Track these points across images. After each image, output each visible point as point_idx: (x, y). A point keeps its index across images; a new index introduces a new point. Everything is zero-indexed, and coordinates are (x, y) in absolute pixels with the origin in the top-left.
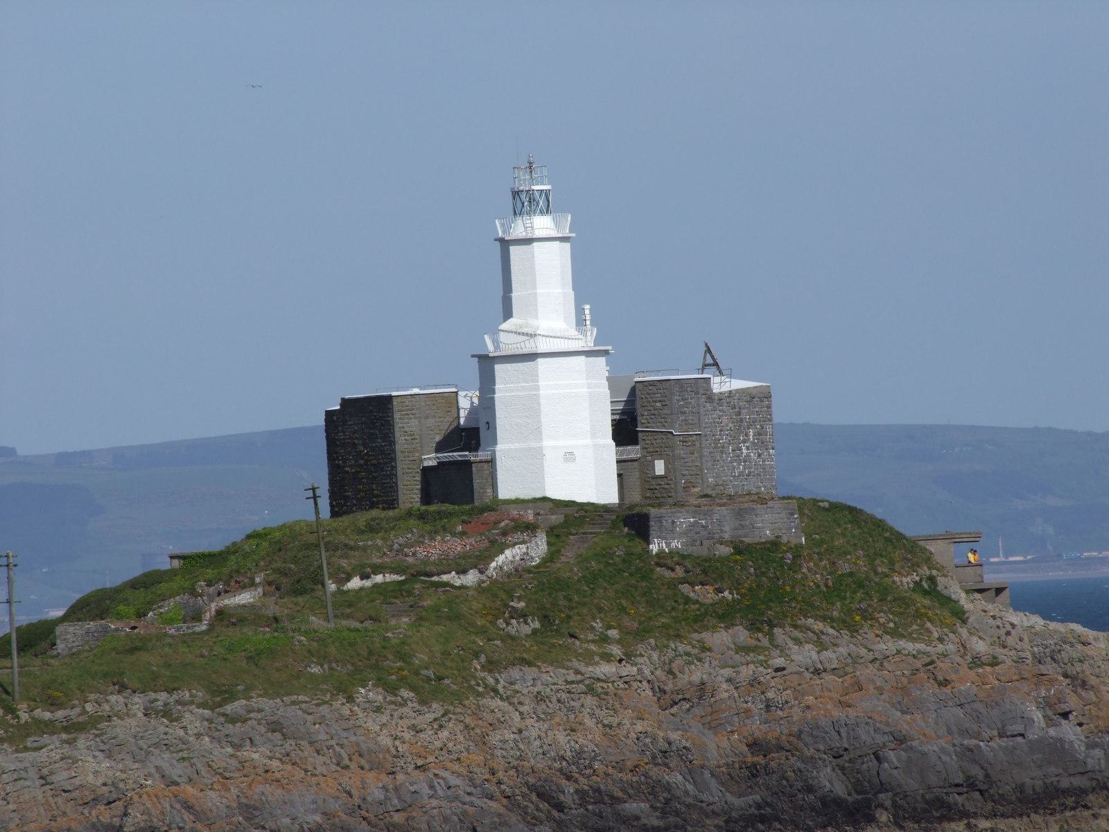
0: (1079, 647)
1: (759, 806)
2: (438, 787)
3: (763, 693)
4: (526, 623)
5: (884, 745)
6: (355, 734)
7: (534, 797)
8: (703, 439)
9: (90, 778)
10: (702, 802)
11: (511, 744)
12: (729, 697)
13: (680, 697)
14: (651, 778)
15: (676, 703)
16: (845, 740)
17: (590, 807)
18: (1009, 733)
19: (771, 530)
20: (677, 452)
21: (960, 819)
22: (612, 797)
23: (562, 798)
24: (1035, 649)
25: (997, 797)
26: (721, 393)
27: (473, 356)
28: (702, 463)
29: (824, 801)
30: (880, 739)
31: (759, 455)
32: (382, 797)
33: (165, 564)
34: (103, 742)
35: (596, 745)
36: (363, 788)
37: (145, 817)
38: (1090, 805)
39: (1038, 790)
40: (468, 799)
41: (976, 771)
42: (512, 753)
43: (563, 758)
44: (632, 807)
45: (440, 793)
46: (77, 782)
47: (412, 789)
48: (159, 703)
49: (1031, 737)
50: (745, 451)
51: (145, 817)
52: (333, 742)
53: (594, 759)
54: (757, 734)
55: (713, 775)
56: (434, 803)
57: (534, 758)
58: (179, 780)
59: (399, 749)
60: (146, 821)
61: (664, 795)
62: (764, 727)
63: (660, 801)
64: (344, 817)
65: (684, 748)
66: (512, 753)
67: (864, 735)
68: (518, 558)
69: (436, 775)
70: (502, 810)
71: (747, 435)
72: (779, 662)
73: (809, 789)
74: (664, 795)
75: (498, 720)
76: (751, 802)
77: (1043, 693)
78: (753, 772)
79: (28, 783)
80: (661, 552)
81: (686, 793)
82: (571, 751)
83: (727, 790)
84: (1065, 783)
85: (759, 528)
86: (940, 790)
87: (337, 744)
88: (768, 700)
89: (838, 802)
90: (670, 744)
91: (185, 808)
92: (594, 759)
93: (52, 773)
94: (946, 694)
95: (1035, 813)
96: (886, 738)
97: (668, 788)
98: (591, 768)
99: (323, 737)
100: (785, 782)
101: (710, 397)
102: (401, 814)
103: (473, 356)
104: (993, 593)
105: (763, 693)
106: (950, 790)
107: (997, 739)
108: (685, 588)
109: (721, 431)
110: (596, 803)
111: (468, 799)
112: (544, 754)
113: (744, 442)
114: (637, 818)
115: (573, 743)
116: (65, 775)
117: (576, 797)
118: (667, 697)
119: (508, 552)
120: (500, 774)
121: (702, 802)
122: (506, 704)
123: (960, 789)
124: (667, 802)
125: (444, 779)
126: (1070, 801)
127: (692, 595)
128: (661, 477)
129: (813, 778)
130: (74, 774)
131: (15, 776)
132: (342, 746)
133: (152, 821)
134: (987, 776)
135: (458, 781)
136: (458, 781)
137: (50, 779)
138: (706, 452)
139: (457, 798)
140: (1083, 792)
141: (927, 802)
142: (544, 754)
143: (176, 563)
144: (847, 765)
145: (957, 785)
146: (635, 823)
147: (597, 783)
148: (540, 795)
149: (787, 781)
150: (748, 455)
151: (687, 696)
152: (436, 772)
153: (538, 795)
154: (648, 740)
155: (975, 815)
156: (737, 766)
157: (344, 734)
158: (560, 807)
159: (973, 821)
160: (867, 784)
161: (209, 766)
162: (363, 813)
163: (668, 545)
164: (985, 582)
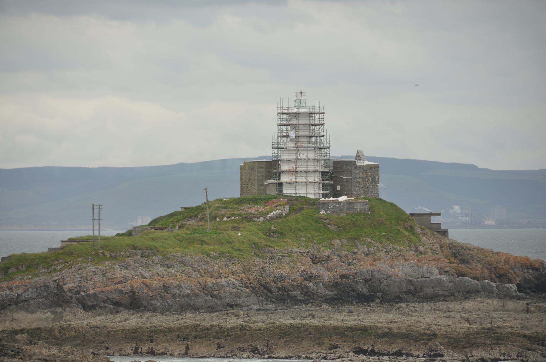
0: (468, 251)
1: (336, 295)
2: (230, 284)
3: (348, 260)
4: (275, 234)
5: (383, 278)
6: (207, 266)
7: (262, 288)
8: (353, 180)
9: (118, 275)
10: (318, 293)
11: (259, 271)
12: (337, 261)
13: (322, 260)
14: (302, 284)
15: (320, 262)
16: (371, 276)
17: (280, 292)
18: (425, 277)
19: (359, 209)
20: (344, 183)
21: (405, 302)
22: (289, 290)
23: (272, 289)
24: (453, 251)
25: (418, 296)
26: (360, 166)
27: (60, 241)
28: (351, 187)
29: (358, 294)
30: (382, 276)
31: (373, 186)
32: (212, 286)
33: (180, 210)
34: (124, 264)
35: (287, 273)
36: (206, 283)
37: (131, 288)
38: (447, 300)
39: (431, 295)
40: (239, 288)
41: (412, 288)
42: (259, 274)
43: (276, 277)
44: (293, 293)
45: (231, 286)
46: (114, 276)
47: (222, 284)
48: (146, 253)
49: (431, 278)
50: (367, 184)
51: (131, 288)
52: (199, 268)
53: (285, 278)
54: (344, 273)
55: (323, 285)
56: (228, 288)
57: (267, 276)
58: (147, 277)
59: (221, 271)
60: (131, 289)
61: (306, 290)
62: (346, 271)
63: (304, 292)
64: (197, 291)
65: (317, 276)
66: (259, 274)
67: (377, 275)
68: (278, 214)
69: (230, 280)
70: (250, 292)
71: (369, 179)
72: (355, 250)
73: (354, 291)
74: (306, 290)
75: (255, 264)
76: (334, 294)
77: (440, 265)
78: (337, 284)
79: (98, 276)
80: (324, 214)
81: (313, 290)
82: (279, 275)
83: (327, 289)
84: (440, 293)
85: (467, 215)
86: (399, 293)
87: (201, 269)
88: (349, 262)
89: (363, 295)
90: (312, 274)
91: (146, 286)
92: (285, 278)
93: (106, 273)
94: (406, 263)
95: (430, 302)
96: (384, 276)
97: (307, 287)
98: (284, 280)
99: (196, 266)
100: (346, 288)
101: (356, 167)
102: (217, 292)
103: (60, 241)
104: (443, 233)
105: (348, 260)
106: (403, 293)
107: (421, 278)
108: (329, 226)
109: (359, 177)
110: (283, 291)
111: (239, 288)
112: (270, 275)
113: (367, 181)
114: (296, 297)
115: (279, 272)
116: (110, 274)
117: (277, 289)
118: (317, 259)
119: (274, 212)
120: (251, 281)
121: (318, 293)
122: (469, 278)
123: (406, 293)
124: (307, 292)
125: (232, 281)
126: (441, 299)
127: (331, 228)
128: (339, 191)
129: (356, 287)
130: (113, 274)
131: (94, 273)
132: (202, 269)
133: (133, 289)
134: (415, 289)
135: (237, 282)
136: (237, 282)
137: (106, 275)
138: (353, 184)
139: (236, 288)
140: (446, 296)
141: (394, 297)
142: (270, 275)
143: (183, 210)
144: (370, 284)
145: (405, 292)
146: (295, 298)
147: (284, 285)
148: (265, 288)
149: (347, 288)
150: (368, 186)
151: (324, 260)
152: (230, 279)
153: (264, 288)
154: (305, 273)
155: (409, 302)
156: (332, 282)
157: (204, 266)
158: (271, 292)
159: (408, 303)
160: (376, 290)
161: (158, 273)
162: (205, 291)
163: (326, 212)
164: (441, 229)
